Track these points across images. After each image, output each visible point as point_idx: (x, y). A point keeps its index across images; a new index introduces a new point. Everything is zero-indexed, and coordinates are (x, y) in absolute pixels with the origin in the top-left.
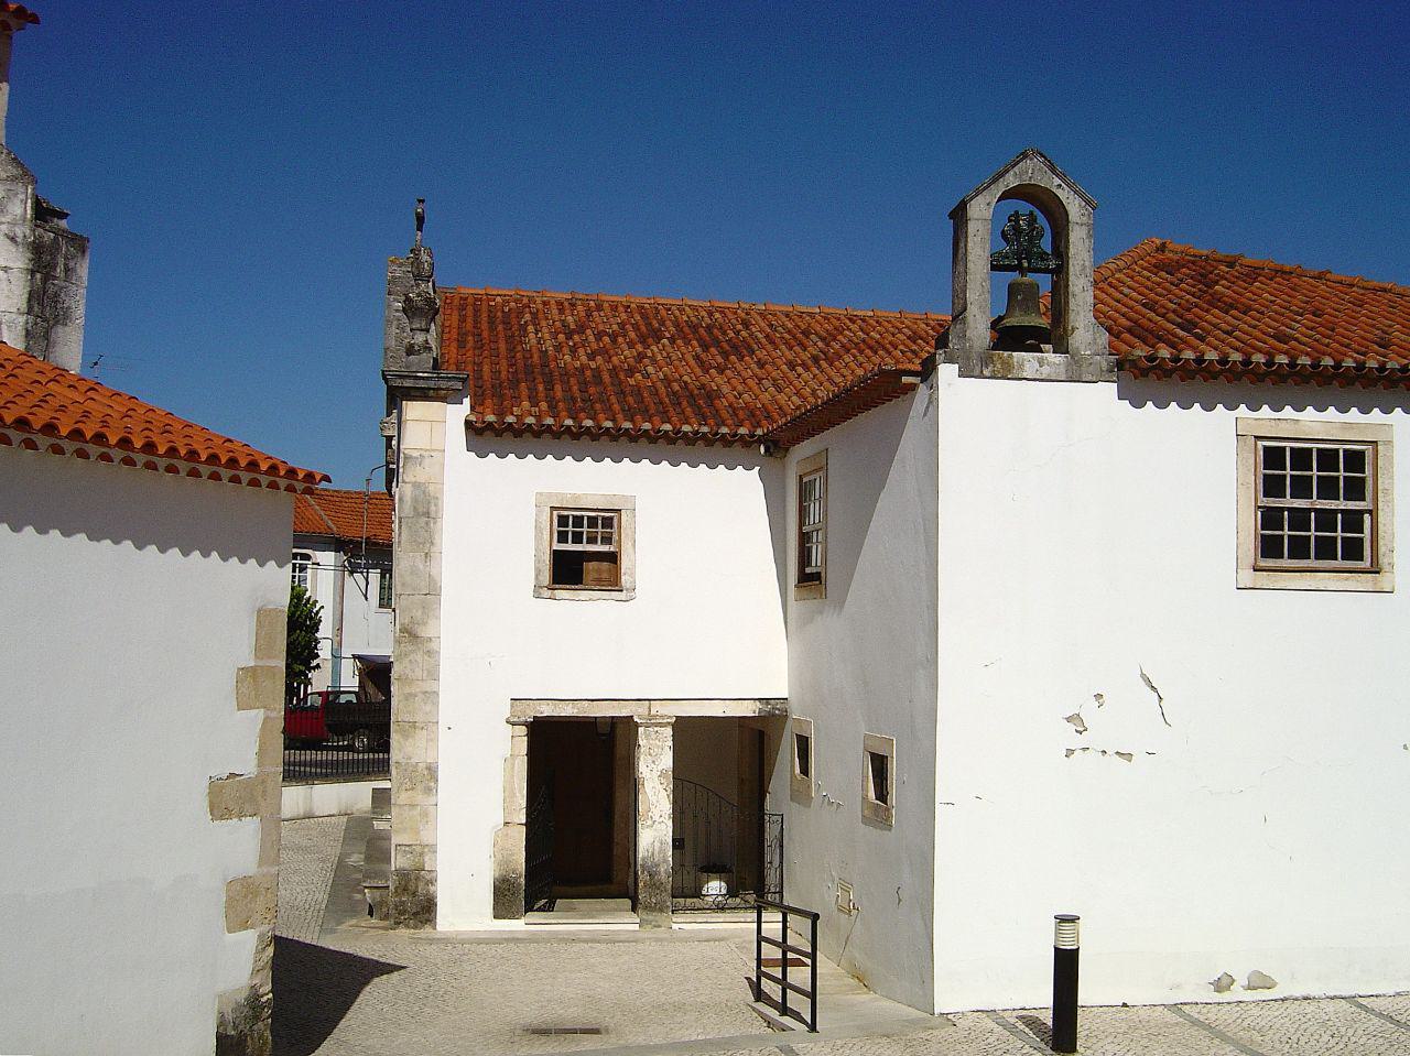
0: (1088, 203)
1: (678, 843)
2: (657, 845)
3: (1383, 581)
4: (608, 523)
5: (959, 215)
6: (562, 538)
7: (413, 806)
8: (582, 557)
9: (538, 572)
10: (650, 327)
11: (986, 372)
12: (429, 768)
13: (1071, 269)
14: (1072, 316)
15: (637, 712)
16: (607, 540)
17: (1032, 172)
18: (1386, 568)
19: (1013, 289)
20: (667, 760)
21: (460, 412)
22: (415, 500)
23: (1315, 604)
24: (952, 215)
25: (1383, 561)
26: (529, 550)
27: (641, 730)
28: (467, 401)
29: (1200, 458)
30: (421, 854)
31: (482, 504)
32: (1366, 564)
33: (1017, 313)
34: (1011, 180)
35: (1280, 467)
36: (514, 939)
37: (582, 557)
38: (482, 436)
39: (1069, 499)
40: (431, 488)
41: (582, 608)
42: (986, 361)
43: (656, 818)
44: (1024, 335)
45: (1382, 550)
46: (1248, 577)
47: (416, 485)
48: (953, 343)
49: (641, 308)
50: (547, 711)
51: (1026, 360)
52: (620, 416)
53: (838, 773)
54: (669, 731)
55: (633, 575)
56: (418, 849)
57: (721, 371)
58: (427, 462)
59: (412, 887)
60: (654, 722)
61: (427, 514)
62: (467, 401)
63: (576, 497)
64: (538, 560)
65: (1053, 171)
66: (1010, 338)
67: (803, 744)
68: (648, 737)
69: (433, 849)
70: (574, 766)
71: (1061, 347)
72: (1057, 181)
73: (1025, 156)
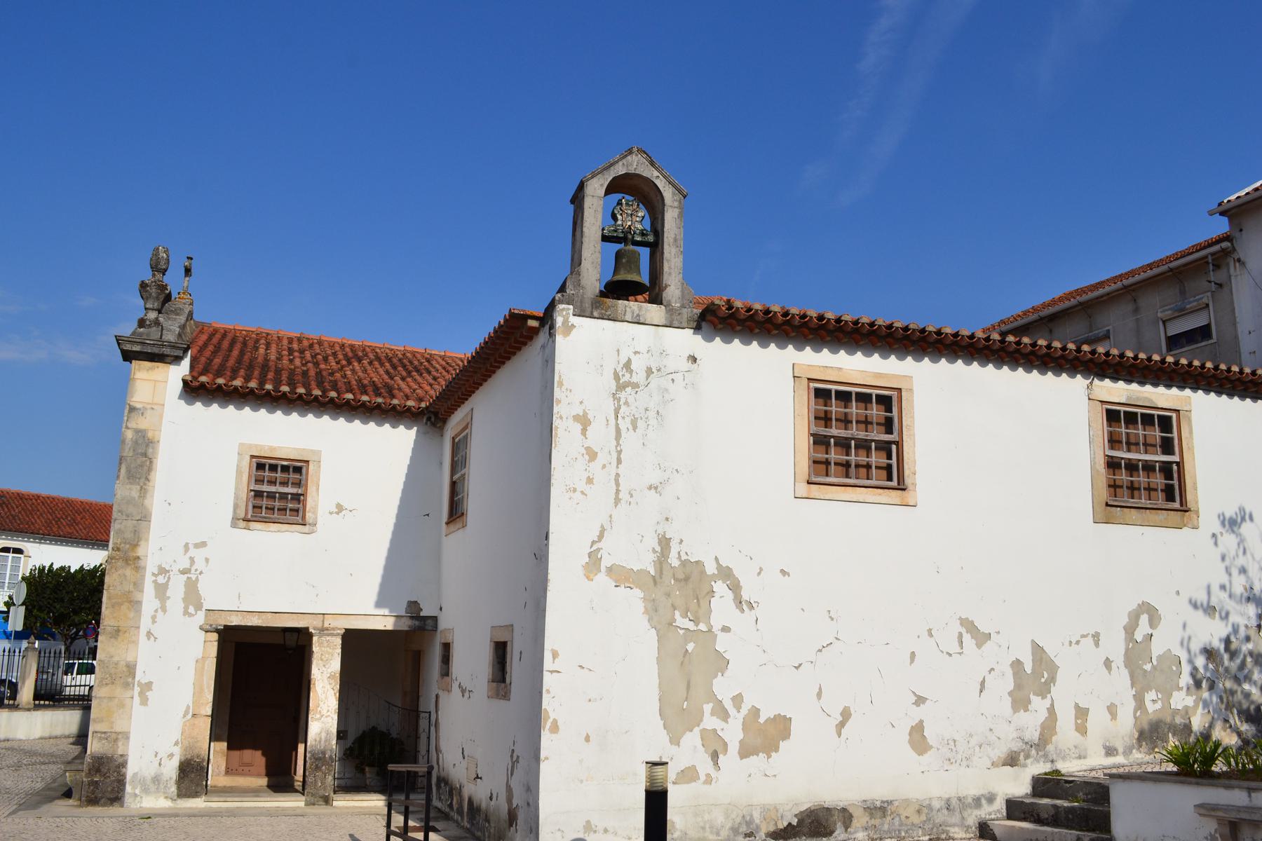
0: (680, 191)
1: (341, 735)
2: (323, 735)
3: (908, 496)
4: (298, 470)
5: (578, 199)
6: (259, 481)
7: (111, 698)
8: (277, 491)
9: (236, 507)
10: (355, 355)
11: (596, 314)
12: (128, 666)
13: (665, 240)
14: (665, 277)
15: (310, 624)
16: (298, 484)
17: (636, 164)
18: (910, 487)
19: (619, 255)
20: (335, 665)
21: (182, 369)
22: (136, 443)
23: (855, 513)
24: (572, 201)
25: (908, 481)
26: (228, 485)
27: (315, 639)
28: (186, 362)
29: (766, 385)
30: (116, 740)
31: (197, 449)
32: (894, 483)
33: (622, 271)
34: (620, 170)
35: (827, 399)
36: (193, 815)
37: (277, 491)
38: (193, 391)
39: (662, 426)
40: (150, 435)
41: (274, 539)
42: (596, 304)
43: (324, 712)
44: (626, 289)
45: (907, 472)
46: (803, 489)
47: (137, 431)
48: (570, 290)
49: (352, 346)
50: (235, 621)
51: (630, 306)
52: (313, 384)
53: (471, 662)
54: (339, 641)
55: (315, 513)
56: (114, 736)
57: (403, 379)
58: (149, 412)
59: (104, 770)
60: (323, 630)
61: (145, 455)
62: (186, 362)
63: (272, 449)
64: (237, 497)
65: (652, 164)
66: (618, 289)
67: (447, 647)
68: (321, 644)
69: (126, 736)
70: (257, 674)
71: (656, 299)
72: (656, 173)
73: (630, 152)
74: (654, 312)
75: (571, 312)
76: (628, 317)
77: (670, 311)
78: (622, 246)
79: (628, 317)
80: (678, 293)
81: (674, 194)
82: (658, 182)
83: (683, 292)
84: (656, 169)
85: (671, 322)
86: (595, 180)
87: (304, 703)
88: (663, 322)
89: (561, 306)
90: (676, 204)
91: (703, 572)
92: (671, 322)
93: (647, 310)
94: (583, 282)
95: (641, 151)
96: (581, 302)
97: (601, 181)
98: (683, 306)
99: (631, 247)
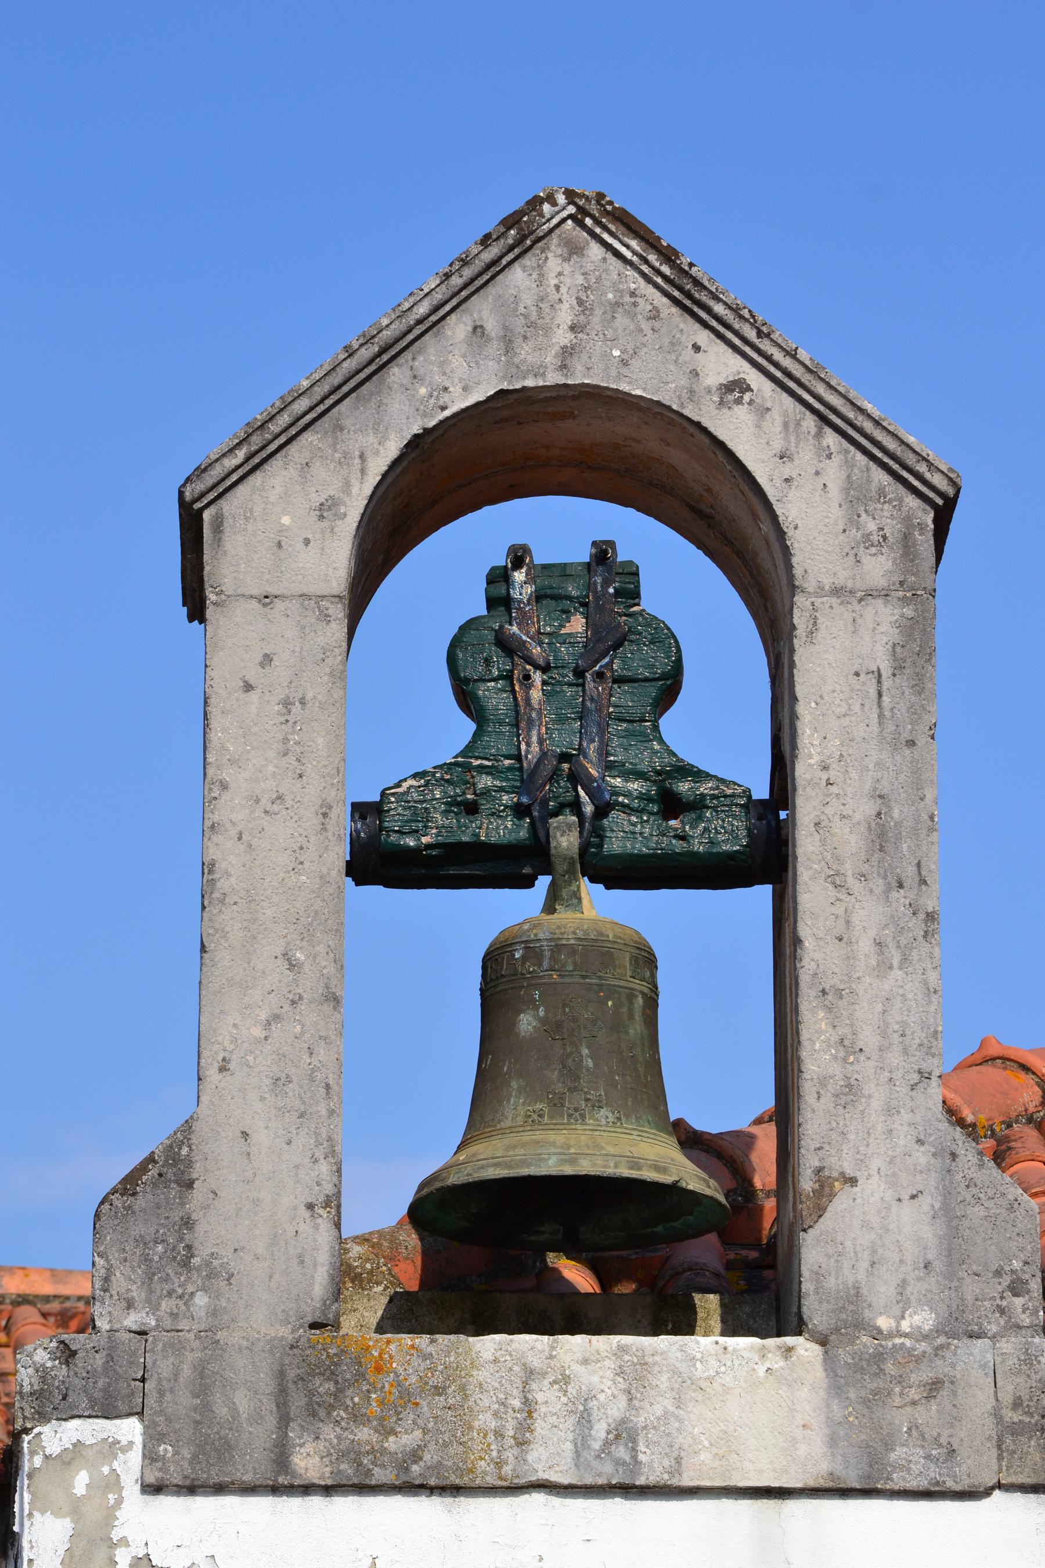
0: (900, 468)
11: (308, 1462)
19: (503, 977)
33: (515, 1107)
34: (454, 377)
51: (571, 1376)
65: (689, 295)
71: (764, 1296)
72: (721, 364)
73: (520, 233)
74: (726, 1387)
75: (130, 1466)
76: (551, 1455)
77: (864, 1367)
78: (516, 907)
79: (551, 1455)
80: (914, 1228)
81: (856, 498)
82: (739, 431)
83: (949, 1214)
84: (721, 330)
85: (875, 1456)
86: (277, 477)
87: (379, 493)
88: (812, 1462)
89: (54, 1437)
90: (878, 568)
91: (56, 1321)
92: (875, 1456)
93: (687, 1387)
94: (212, 1235)
95: (604, 217)
96: (204, 1383)
97: (326, 481)
98: (960, 1327)
99: (600, 905)
